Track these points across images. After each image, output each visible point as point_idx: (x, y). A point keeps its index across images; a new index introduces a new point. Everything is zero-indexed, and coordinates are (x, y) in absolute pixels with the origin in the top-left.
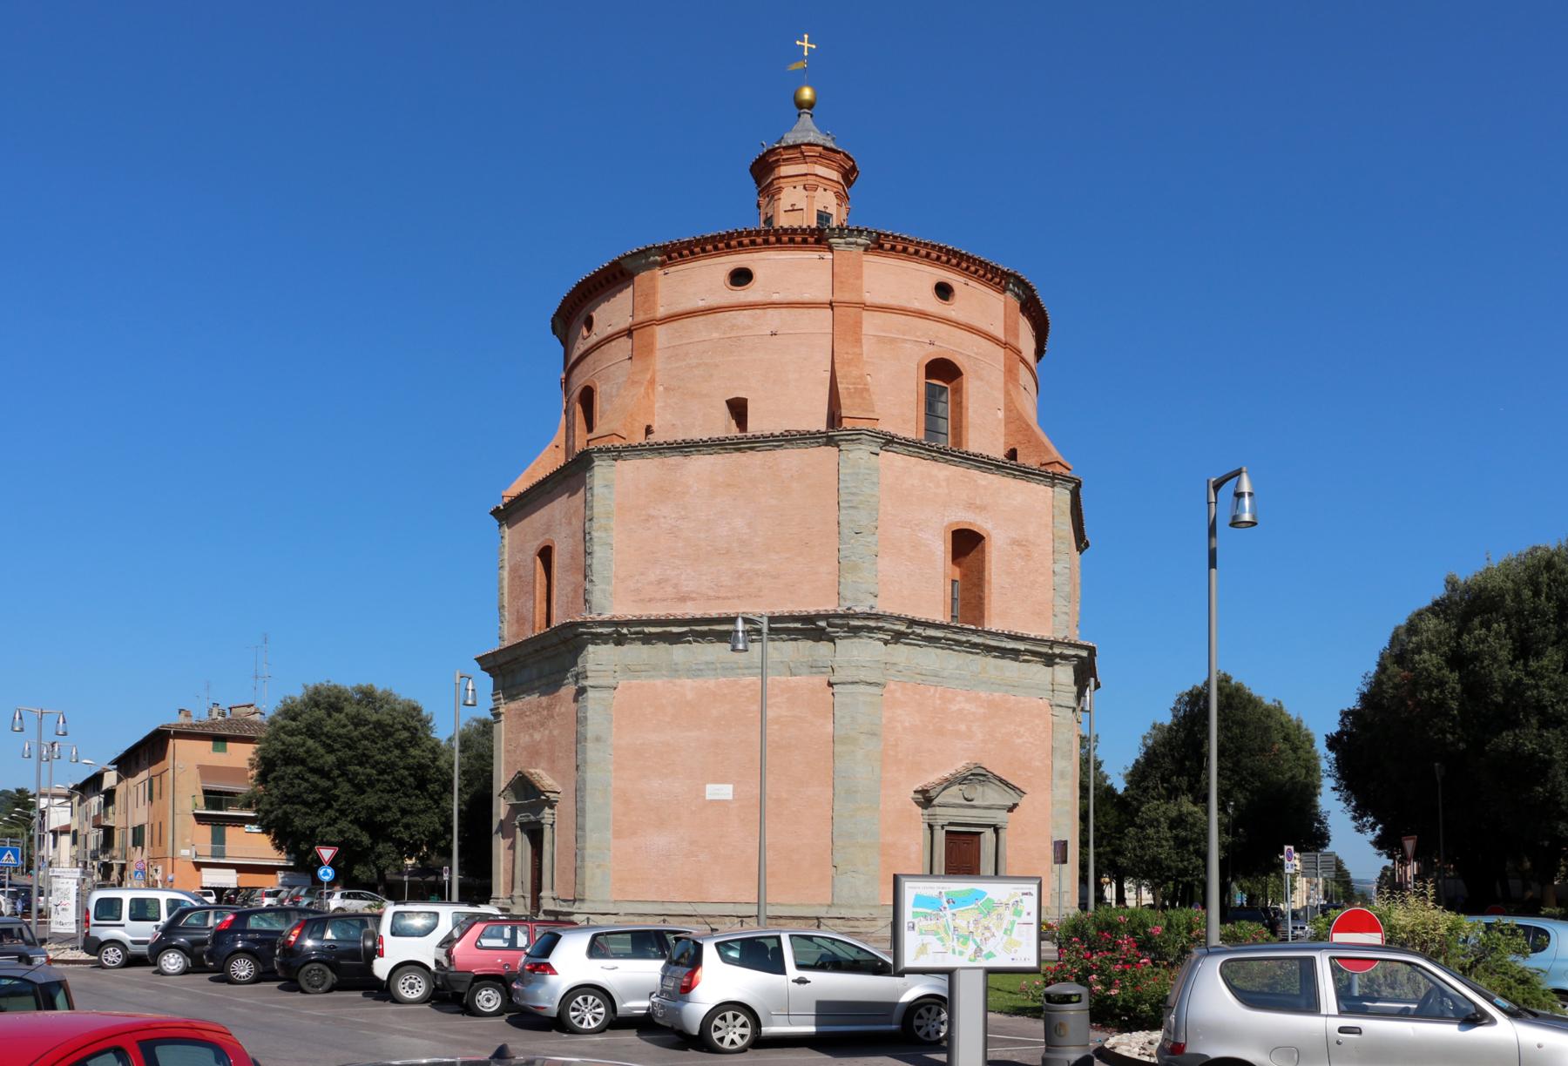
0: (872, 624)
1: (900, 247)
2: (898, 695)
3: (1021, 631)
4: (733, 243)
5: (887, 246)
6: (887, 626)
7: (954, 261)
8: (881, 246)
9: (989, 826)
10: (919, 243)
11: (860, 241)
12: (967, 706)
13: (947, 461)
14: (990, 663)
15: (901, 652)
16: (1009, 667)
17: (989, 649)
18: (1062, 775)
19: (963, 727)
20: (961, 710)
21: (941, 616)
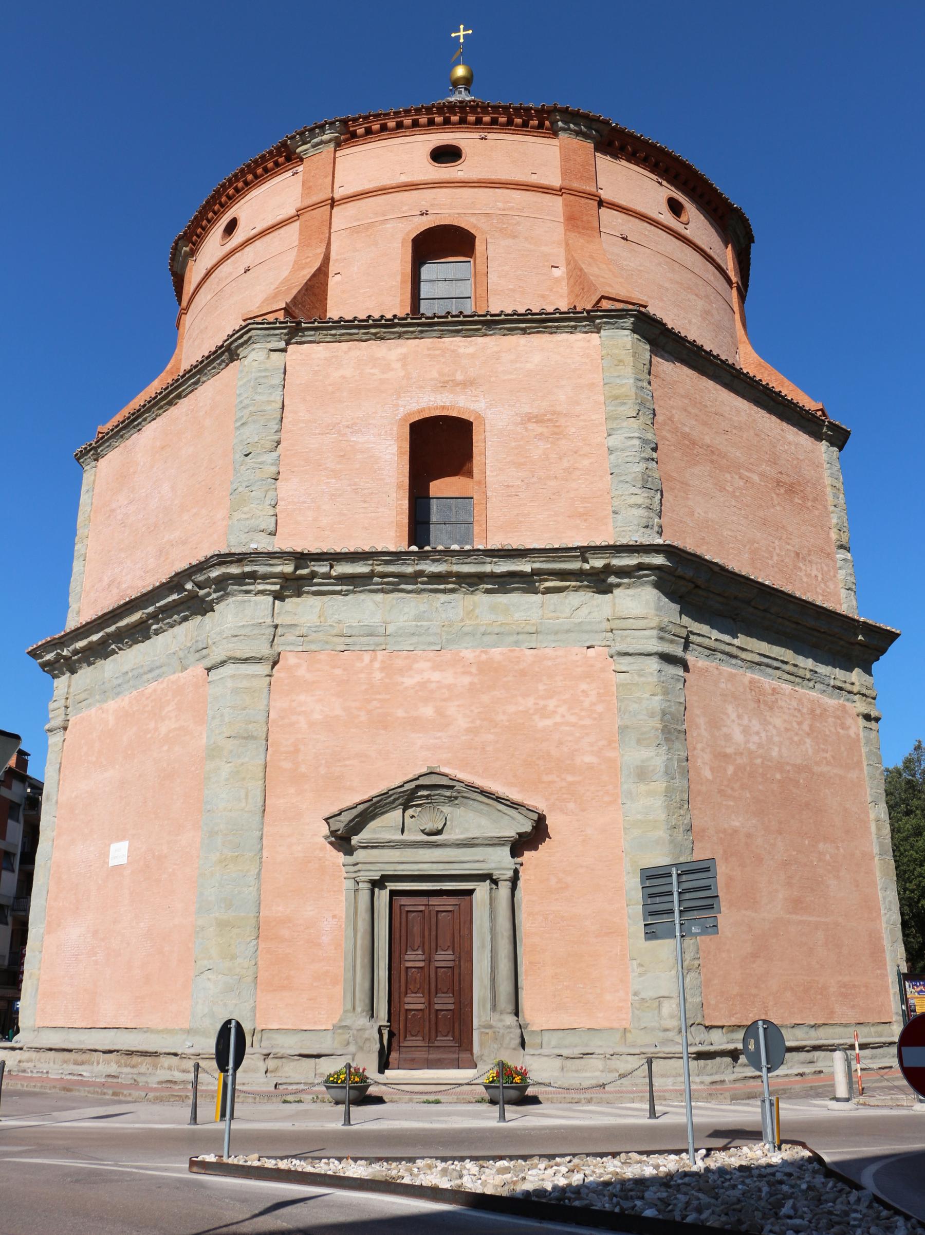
0: (234, 570)
1: (376, 127)
2: (302, 672)
3: (515, 543)
4: (224, 199)
5: (360, 131)
6: (262, 569)
7: (455, 118)
8: (354, 135)
9: (482, 878)
10: (397, 114)
11: (325, 137)
12: (436, 676)
13: (400, 336)
14: (483, 605)
15: (305, 610)
16: (522, 606)
17: (472, 581)
18: (642, 774)
19: (428, 711)
20: (423, 685)
21: (403, 546)
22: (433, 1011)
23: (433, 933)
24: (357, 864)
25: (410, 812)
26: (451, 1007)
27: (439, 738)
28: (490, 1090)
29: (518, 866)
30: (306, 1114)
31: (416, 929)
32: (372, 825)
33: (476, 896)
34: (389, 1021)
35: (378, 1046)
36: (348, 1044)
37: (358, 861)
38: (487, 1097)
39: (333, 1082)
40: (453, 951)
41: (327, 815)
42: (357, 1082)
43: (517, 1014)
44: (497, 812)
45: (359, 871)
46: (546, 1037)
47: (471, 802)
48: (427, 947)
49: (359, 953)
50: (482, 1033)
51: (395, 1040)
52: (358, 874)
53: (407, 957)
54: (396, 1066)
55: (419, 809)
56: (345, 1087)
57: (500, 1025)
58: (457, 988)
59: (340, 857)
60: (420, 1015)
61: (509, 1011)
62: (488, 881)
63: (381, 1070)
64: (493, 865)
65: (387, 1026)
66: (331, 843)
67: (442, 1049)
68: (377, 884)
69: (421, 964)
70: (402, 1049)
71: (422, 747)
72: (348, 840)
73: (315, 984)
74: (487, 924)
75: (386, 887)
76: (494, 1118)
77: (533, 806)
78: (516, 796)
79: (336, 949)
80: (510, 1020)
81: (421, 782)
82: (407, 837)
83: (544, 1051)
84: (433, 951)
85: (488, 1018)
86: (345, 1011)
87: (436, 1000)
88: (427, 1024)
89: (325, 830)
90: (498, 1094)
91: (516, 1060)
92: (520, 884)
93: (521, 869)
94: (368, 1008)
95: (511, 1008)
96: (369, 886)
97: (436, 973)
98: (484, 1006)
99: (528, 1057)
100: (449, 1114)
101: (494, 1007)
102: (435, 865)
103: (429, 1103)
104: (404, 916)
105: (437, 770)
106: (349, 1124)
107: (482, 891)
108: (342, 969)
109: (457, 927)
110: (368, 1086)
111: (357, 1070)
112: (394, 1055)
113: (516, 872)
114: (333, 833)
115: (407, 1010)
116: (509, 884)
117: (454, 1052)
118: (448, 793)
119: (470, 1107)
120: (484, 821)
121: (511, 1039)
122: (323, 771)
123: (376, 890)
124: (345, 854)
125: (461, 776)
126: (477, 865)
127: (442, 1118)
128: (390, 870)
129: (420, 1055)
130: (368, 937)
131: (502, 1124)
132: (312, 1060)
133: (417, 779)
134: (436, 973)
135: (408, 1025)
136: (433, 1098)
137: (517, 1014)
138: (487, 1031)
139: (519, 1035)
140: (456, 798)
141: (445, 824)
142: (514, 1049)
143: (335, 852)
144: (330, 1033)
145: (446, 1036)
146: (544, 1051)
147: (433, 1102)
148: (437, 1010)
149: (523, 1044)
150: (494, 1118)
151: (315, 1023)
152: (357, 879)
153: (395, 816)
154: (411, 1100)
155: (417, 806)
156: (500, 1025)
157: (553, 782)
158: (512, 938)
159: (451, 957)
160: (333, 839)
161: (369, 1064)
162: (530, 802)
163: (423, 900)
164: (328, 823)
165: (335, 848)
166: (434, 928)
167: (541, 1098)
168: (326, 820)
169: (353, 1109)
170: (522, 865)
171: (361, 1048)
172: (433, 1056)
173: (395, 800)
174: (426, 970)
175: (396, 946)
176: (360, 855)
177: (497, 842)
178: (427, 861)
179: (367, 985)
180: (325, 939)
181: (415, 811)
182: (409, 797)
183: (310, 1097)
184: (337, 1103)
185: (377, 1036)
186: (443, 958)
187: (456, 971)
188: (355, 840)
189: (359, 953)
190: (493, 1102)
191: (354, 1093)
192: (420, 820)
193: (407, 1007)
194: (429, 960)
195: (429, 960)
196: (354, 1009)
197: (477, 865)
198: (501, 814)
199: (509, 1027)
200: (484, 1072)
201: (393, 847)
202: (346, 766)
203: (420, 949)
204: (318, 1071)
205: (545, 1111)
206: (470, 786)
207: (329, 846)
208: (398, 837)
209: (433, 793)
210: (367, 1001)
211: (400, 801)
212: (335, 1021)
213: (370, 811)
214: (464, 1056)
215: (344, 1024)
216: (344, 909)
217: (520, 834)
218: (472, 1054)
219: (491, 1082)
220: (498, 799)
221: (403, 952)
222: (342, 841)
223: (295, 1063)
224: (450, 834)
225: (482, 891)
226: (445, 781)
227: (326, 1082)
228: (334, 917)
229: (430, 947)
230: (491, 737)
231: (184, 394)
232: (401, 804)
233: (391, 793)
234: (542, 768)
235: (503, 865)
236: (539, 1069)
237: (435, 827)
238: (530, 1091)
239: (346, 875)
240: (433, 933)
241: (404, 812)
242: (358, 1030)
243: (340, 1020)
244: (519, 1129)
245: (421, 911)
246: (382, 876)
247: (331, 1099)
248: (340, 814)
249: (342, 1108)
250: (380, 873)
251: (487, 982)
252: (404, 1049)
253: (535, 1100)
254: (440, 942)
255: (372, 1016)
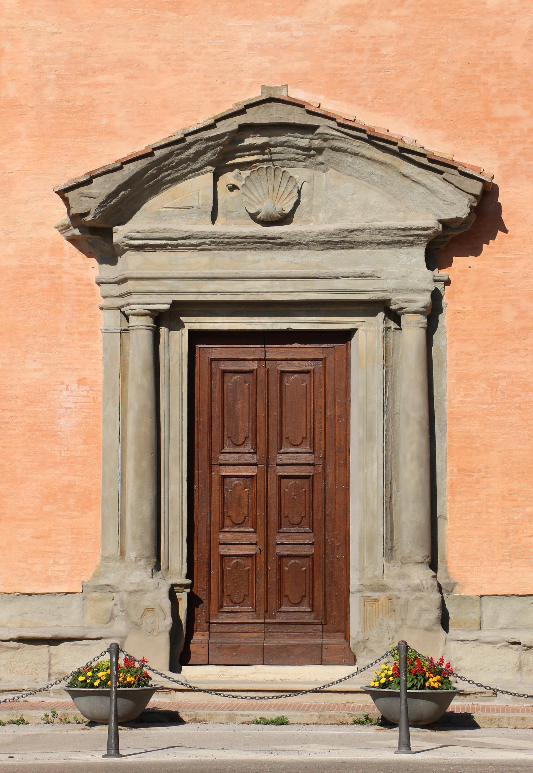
22: (273, 559)
23: (274, 413)
24: (124, 280)
25: (228, 178)
26: (308, 551)
27: (287, 28)
28: (382, 701)
29: (440, 286)
30: (34, 741)
31: (241, 407)
32: (154, 204)
33: (358, 343)
34: (189, 576)
35: (169, 621)
36: (112, 618)
37: (127, 274)
38: (376, 714)
39: (84, 684)
40: (313, 447)
41: (62, 185)
42: (130, 685)
43: (433, 565)
44: (400, 179)
45: (129, 294)
46: (489, 608)
47: (350, 159)
48: (261, 438)
49: (131, 448)
50: (366, 599)
51: (200, 611)
52: (128, 300)
53: (223, 459)
54: (204, 659)
55: (246, 173)
56: (108, 694)
57: (400, 584)
58: (318, 516)
59: (92, 268)
60: (248, 565)
61: (419, 559)
62: (381, 315)
63: (176, 665)
64: (390, 284)
65: (186, 586)
66: (72, 240)
67: (290, 629)
68: (165, 319)
69: (251, 471)
70: (214, 628)
71: (250, 48)
72: (106, 233)
73: (46, 509)
74: (378, 397)
75: (181, 325)
76: (390, 747)
77: (473, 168)
78: (438, 147)
79: (85, 443)
80: (421, 575)
81: (253, 117)
82: (222, 227)
83: (486, 634)
84: (274, 446)
85: (379, 572)
86: (106, 559)
87: (279, 538)
88: (262, 582)
89: (61, 215)
90: (397, 707)
91: (432, 647)
92: (444, 320)
93: (446, 292)
94: (149, 552)
95: (421, 553)
96: (149, 322)
97: (280, 487)
98: (371, 549)
99: (453, 645)
100: (304, 741)
101: (390, 552)
102: (277, 282)
103: (267, 723)
104: (217, 380)
105: (283, 95)
106: (117, 754)
107: (368, 332)
108: (99, 480)
109: (320, 402)
110: (153, 690)
111: (130, 661)
112: (199, 640)
113: (436, 296)
114: (76, 219)
115: (223, 556)
116: (422, 320)
117: (313, 635)
118: (303, 142)
119: (344, 731)
120: (374, 197)
121: (422, 610)
122: (51, 94)
123: (163, 331)
124: (101, 261)
125: (329, 106)
126: (360, 284)
127: (286, 747)
128: (189, 293)
129: (249, 638)
130: (149, 421)
131: (404, 757)
132: (44, 649)
133: (241, 112)
134: (280, 487)
135: (227, 584)
136: (274, 712)
137: (433, 565)
138: (376, 595)
139: (438, 603)
140: (320, 151)
141: (297, 203)
142: (428, 629)
143: (80, 258)
144: (77, 598)
145: (297, 604)
146: (486, 634)
147: (273, 723)
148: (281, 557)
149: (444, 621)
150: (390, 747)
151: (48, 580)
152: (127, 310)
153: (198, 186)
154: (231, 719)
155: (242, 166)
156: (400, 584)
157: (517, 119)
158: (425, 424)
159: (309, 459)
160: (77, 232)
161: (155, 653)
162: (466, 158)
163: (255, 350)
164: (66, 201)
165: (81, 250)
166: (274, 404)
167: (478, 718)
168: (62, 193)
169: (124, 733)
170: (447, 283)
171: (137, 626)
172: (274, 641)
173: (199, 154)
174: (260, 482)
175: (201, 438)
176: (131, 263)
177: (401, 238)
178: (262, 274)
179: (147, 509)
180: (65, 425)
181: (238, 177)
182: (228, 146)
183: (41, 714)
184: (92, 723)
185: (167, 604)
186: (293, 459)
187: (318, 484)
188: (120, 233)
189: (131, 448)
190: (386, 723)
191: (125, 704)
192: (249, 194)
193: (223, 550)
194: (266, 464)
195: (266, 464)
196: (122, 553)
197: (360, 284)
198: (408, 182)
199: (418, 589)
200: (374, 667)
201: (195, 248)
202: (98, 85)
203: (249, 443)
204: (55, 669)
205: (485, 740)
206: (347, 127)
207: (68, 246)
208: (205, 227)
209: (274, 140)
210: (148, 539)
211: (209, 156)
212: (86, 577)
213: (149, 176)
214: (334, 641)
215: (104, 581)
216: (101, 367)
217: (445, 223)
218: (347, 638)
219: (384, 686)
220: (404, 153)
221: (216, 447)
222: (95, 235)
223: (11, 653)
224: (307, 222)
225: (368, 332)
226: (297, 117)
227: (71, 685)
228: (81, 382)
229: (267, 439)
230: (391, 26)
231: (202, 247)
232: (210, 163)
233: (189, 139)
234: (494, 90)
235: (411, 283)
236: (474, 663)
237: (279, 208)
238: (457, 705)
239: (103, 302)
240: (274, 413)
241: (216, 179)
242: (131, 593)
243: (95, 576)
244: (436, 765)
245: (250, 372)
246: (175, 304)
247: (81, 717)
248: (88, 182)
249: (102, 731)
250: (170, 299)
251: (377, 505)
252: (219, 628)
253: (466, 722)
254: (287, 429)
255: (157, 567)
